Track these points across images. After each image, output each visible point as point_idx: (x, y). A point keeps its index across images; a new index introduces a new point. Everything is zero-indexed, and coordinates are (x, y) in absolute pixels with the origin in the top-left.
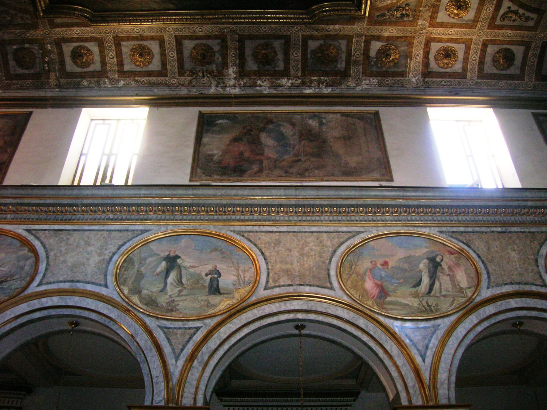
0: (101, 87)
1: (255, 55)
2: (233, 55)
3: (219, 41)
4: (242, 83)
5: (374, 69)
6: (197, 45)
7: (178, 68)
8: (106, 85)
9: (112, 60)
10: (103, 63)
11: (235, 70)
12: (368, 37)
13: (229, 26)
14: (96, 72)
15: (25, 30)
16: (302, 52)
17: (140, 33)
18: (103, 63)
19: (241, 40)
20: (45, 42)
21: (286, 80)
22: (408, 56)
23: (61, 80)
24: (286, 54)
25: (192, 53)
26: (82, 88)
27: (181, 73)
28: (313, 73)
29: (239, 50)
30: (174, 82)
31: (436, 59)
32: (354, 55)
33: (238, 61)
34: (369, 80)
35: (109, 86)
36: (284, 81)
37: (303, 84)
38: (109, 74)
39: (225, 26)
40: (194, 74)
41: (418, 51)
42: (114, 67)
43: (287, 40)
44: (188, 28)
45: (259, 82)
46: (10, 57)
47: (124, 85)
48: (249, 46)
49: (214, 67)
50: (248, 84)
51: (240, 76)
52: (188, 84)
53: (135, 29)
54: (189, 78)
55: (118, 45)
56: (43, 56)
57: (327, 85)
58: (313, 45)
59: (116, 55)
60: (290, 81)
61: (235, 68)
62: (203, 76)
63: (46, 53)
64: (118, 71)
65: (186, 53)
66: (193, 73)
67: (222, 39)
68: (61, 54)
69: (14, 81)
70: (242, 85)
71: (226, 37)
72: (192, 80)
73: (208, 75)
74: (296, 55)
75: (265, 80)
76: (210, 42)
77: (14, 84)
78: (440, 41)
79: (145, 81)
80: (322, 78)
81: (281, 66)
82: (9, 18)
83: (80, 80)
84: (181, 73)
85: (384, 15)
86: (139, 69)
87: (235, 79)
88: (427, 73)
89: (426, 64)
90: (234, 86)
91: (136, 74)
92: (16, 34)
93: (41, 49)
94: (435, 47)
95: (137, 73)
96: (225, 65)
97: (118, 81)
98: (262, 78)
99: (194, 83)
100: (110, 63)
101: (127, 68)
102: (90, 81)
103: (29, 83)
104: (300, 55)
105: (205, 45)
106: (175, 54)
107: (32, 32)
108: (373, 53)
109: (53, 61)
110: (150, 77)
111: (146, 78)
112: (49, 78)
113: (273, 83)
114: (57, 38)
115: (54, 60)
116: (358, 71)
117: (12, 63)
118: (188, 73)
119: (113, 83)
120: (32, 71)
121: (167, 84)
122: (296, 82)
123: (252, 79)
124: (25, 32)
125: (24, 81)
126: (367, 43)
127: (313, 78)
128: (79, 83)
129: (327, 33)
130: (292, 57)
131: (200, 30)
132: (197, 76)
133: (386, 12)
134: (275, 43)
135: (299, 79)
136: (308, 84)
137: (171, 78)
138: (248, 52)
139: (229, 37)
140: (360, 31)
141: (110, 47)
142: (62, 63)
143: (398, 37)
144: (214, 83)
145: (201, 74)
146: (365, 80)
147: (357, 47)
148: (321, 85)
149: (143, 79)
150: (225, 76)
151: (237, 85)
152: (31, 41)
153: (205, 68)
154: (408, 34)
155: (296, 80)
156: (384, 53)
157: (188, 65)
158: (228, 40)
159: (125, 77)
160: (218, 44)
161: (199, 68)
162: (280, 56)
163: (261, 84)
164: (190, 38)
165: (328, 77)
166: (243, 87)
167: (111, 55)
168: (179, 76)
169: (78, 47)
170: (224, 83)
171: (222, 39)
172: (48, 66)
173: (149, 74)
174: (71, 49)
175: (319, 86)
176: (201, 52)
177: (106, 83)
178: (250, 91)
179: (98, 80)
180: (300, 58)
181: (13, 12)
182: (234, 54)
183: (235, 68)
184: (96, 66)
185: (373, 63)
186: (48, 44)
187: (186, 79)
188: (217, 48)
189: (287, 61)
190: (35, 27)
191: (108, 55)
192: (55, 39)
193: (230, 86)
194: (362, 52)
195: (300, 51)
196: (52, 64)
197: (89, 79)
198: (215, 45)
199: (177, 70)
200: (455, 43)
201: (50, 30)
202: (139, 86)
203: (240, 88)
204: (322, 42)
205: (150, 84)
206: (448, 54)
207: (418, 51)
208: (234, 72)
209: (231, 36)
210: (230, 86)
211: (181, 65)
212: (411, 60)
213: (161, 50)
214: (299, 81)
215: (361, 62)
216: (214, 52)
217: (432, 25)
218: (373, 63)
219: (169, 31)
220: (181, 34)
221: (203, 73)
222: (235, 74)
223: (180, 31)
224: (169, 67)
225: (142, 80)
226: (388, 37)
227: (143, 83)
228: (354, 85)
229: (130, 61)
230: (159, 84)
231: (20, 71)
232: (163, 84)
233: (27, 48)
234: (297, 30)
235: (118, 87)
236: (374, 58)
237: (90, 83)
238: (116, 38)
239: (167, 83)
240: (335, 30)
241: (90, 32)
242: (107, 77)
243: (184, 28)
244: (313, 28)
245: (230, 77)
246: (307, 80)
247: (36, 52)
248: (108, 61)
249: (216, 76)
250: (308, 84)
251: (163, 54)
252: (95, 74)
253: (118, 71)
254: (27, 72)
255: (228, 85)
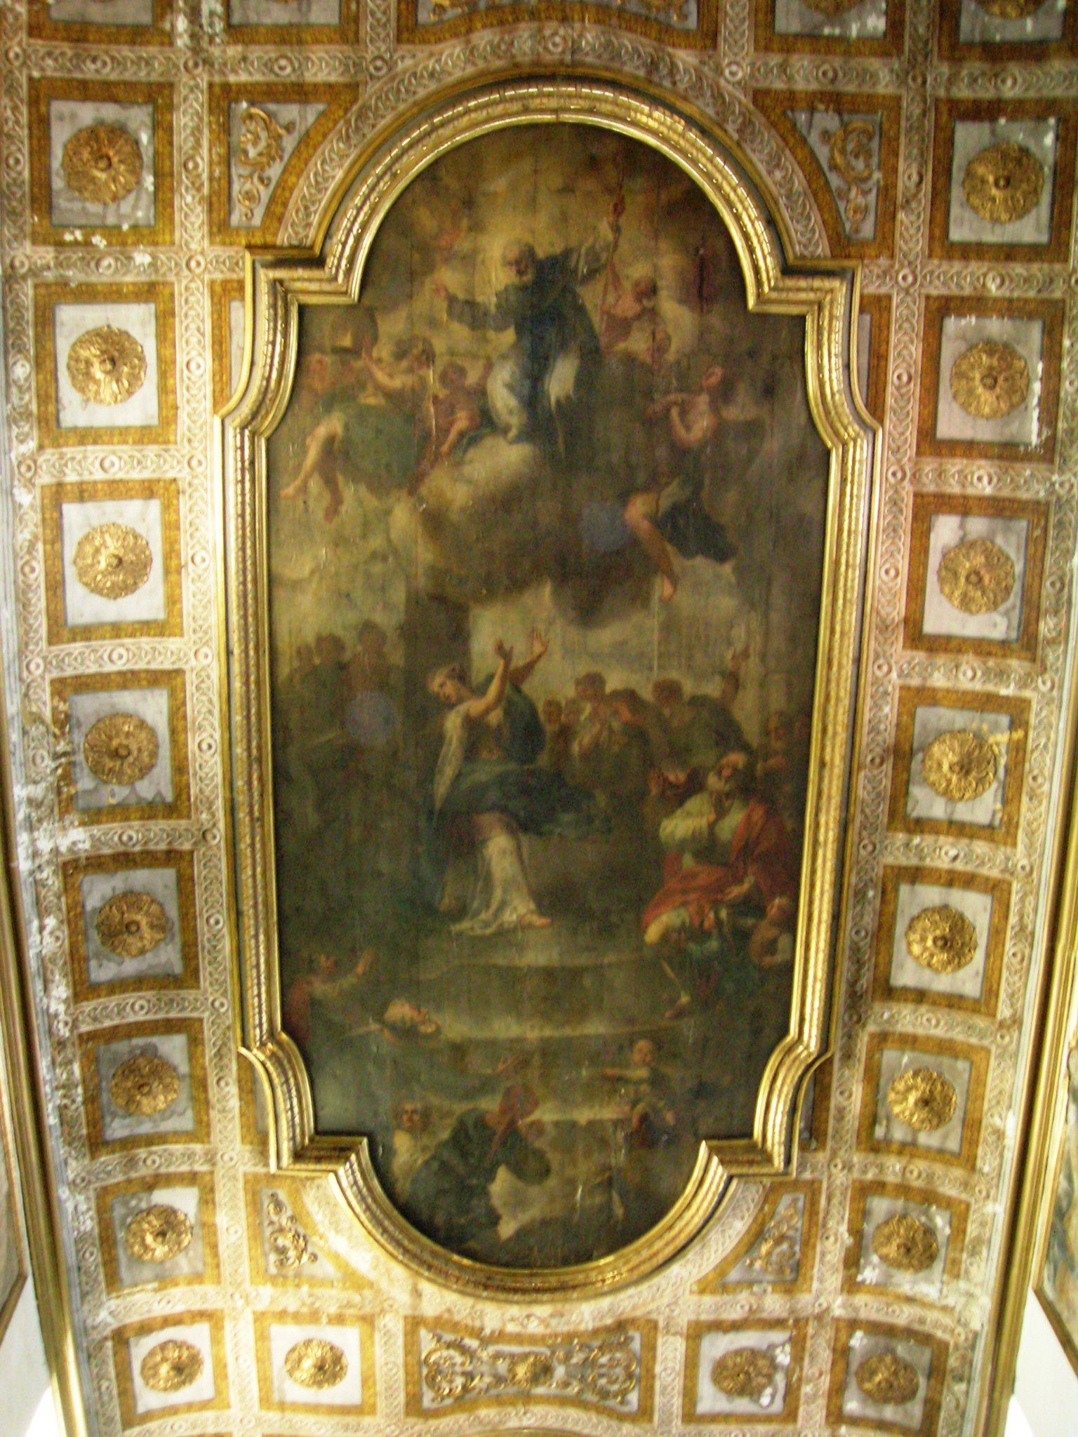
0: (10, 426)
1: (130, 898)
2: (125, 838)
3: (169, 796)
4: (45, 875)
5: (119, 1212)
6: (152, 732)
7: (77, 677)
8: (15, 442)
9: (97, 463)
10: (88, 436)
11: (80, 846)
12: (208, 1178)
13: (221, 825)
14: (58, 412)
15: (206, 191)
16: (150, 1022)
17: (191, 565)
18: (88, 436)
19: (171, 857)
20: (161, 248)
21: (64, 996)
22: (164, 1280)
23: (30, 282)
24: (138, 983)
25: (128, 716)
26: (6, 358)
27: (62, 688)
28: (91, 1060)
29: (142, 852)
30: (33, 667)
31: (163, 1347)
32: (151, 1153)
33: (106, 851)
34: (89, 1209)
35: (13, 455)
36: (61, 990)
37: (61, 1044)
38: (49, 454)
39: (221, 815)
40: (62, 728)
41: (179, 1299)
42: (74, 470)
43: (188, 976)
44: (210, 712)
45: (51, 922)
46: (110, 112)
47: (21, 506)
48: (159, 880)
49: (85, 782)
50: (43, 892)
51: (65, 864)
52: (31, 713)
53: (203, 553)
54: (48, 715)
55: (148, 490)
56: (112, 232)
57: (62, 1110)
58: (173, 1047)
59: (114, 482)
60: (62, 1008)
61: (87, 846)
62: (56, 756)
63: (122, 241)
64: (60, 485)
65: (127, 700)
66: (64, 722)
67: (176, 806)
68: (114, 295)
69: (24, 110)
70: (39, 876)
71: (180, 817)
72: (43, 722)
73: (60, 771)
74: (138, 1007)
75: (57, 938)
76: (163, 768)
77: (15, 109)
78: (216, 1340)
79: (32, 577)
80: (80, 1090)
81: (102, 972)
82: (252, 153)
83: (32, 352)
84: (62, 688)
85: (279, 1206)
86: (70, 552)
87: (55, 851)
88: (121, 1338)
89: (145, 1329)
90: (35, 854)
91: (53, 544)
92: (192, 158)
93: (135, 227)
94: (197, 1335)
95: (57, 546)
96: (94, 816)
97: (30, 484)
98: (65, 928)
99: (34, 731)
100: (85, 458)
101: (72, 512)
102: (29, 388)
103: (19, 168)
104: (141, 1017)
105: (154, 754)
106: (120, 666)
107: (199, 217)
108: (161, 1197)
109: (93, 264)
110: (47, 589)
111: (42, 578)
112: (34, 243)
113: (53, 961)
114: (172, 295)
115: (98, 265)
116: (109, 1173)
117: (87, 113)
118: (62, 707)
119: (23, 469)
120: (58, 183)
121: (27, 645)
122: (61, 1025)
123: (59, 898)
124: (199, 190)
125: (26, 150)
126: (192, 1179)
127: (76, 1068)
128: (21, 350)
129: (212, 1080)
130: (131, 997)
131: (204, 746)
132: (55, 736)
133: (289, 1213)
134: (170, 948)
135: (71, 1031)
136: (59, 1059)
137: (45, 658)
138: (140, 878)
139: (183, 823)
140: (226, 1158)
141: (139, 463)
142: (88, 294)
143: (214, 1247)
144: (38, 791)
145: (62, 747)
146: (88, 1199)
147: (176, 1156)
148: (61, 1092)
149: (39, 567)
150: (61, 819)
151: (37, 862)
152: (163, 200)
153: (80, 757)
154: (226, 1269)
155: (66, 1024)
156: (169, 1224)
157: (88, 706)
158: (173, 823)
159: (43, 507)
160: (159, 793)
161: (79, 738)
162: (130, 967)
163: (48, 929)
164: (177, 714)
165: (84, 1103)
166: (36, 881)
167: (113, 464)
168: (53, 682)
169: (142, 359)
170: (40, 821)
171: (176, 806)
172: (76, 243)
173: (56, 587)
174: (136, 333)
175: (57, 1088)
176: (134, 747)
177: (22, 442)
178: (26, 898)
179: (31, 414)
180: (132, 1019)
181: (274, 171)
182: (130, 838)
183: (87, 846)
184: (75, 411)
185: (133, 1203)
186: (154, 257)
187: (45, 703)
188: (146, 789)
189: (118, 986)
190: (220, 228)
191: (114, 453)
192: (172, 284)
193: (33, 841)
194: (163, 1170)
195: (150, 1017)
196: (83, 258)
197: (34, 385)
198: (157, 784)
199: (69, 672)
200: (215, 1377)
201: (207, 277)
202: (16, 556)
203: (32, 873)
204: (184, 1068)
205: (24, 593)
206: (185, 1370)
207: (179, 1299)
208: (74, 843)
209: (187, 830)
210: (33, 841)
211: (83, 684)
212: (155, 1290)
213: (133, 623)
214: (64, 1032)
215: (133, 1175)
216: (131, 783)
217: (259, 1317)
218: (133, 1203)
219: (201, 656)
220: (190, 689)
221: (65, 754)
222: (70, 850)
223: (198, 688)
224: (77, 647)
225: (34, 564)
226: (214, 1225)
227: (27, 569)
228: (71, 1176)
229: (95, 523)
230: (25, 620)
231: (60, 136)
232: (27, 633)
233: (139, 182)
234: (217, 1004)
235: (12, 487)
236: (149, 1201)
237: (20, 388)
238: (173, 487)
239: (31, 647)
240: (224, 1098)
241: (194, 410)
242: (41, 447)
243: (210, 701)
244: (224, 1044)
245: (59, 834)
246: (69, 1051)
247: (125, 207)
248: (94, 452)
249: (59, 793)
250: (59, 1059)
251: (117, 630)
252: (51, 408)
253: (60, 485)
254: (56, 164)
255: (36, 834)
